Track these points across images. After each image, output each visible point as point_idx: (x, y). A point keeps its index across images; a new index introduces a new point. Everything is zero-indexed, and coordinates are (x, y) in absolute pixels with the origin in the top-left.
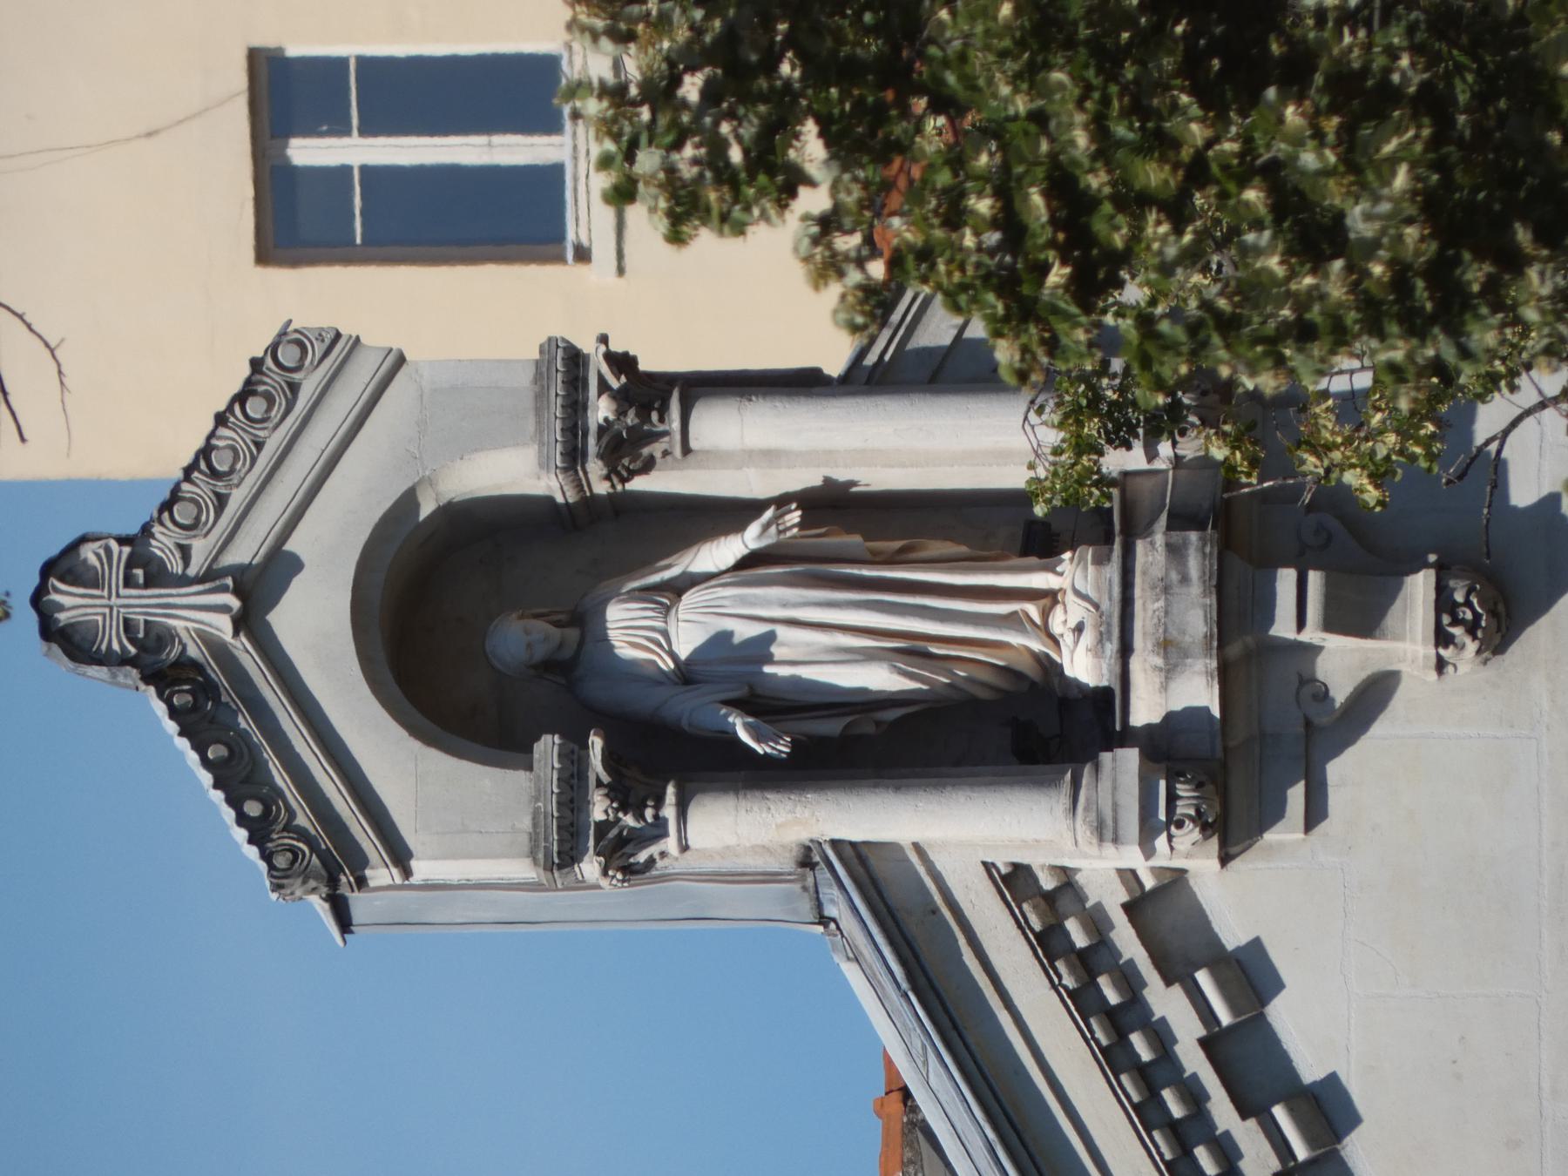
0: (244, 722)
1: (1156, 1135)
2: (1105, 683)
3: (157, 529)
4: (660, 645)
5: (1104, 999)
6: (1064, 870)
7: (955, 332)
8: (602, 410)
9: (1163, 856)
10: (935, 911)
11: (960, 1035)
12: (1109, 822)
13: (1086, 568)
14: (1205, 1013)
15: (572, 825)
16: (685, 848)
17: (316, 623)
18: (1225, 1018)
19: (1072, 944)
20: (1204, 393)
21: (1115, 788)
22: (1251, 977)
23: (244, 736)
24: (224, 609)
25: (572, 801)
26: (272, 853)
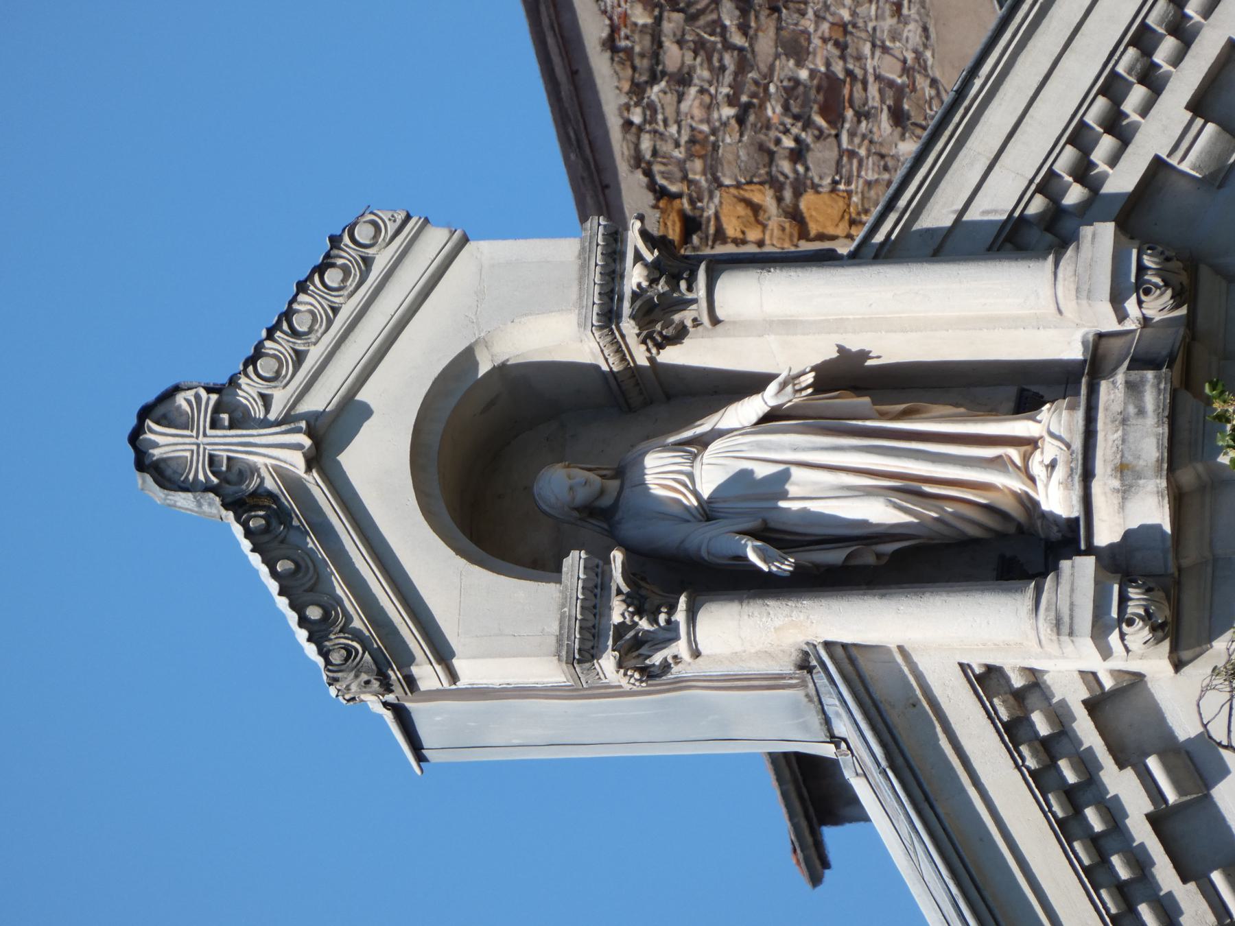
0: (312, 543)
1: (1104, 893)
2: (1075, 514)
3: (243, 381)
4: (686, 486)
5: (1063, 778)
6: (1032, 671)
7: (954, 216)
8: (635, 276)
9: (1120, 661)
10: (915, 704)
11: (932, 807)
12: (1066, 619)
13: (1060, 414)
14: (1154, 792)
15: (594, 627)
16: (696, 654)
17: (380, 463)
18: (1171, 796)
19: (1036, 733)
20: (1168, 259)
21: (1072, 590)
22: (1198, 764)
23: (310, 554)
24: (298, 447)
25: (595, 607)
26: (329, 651)
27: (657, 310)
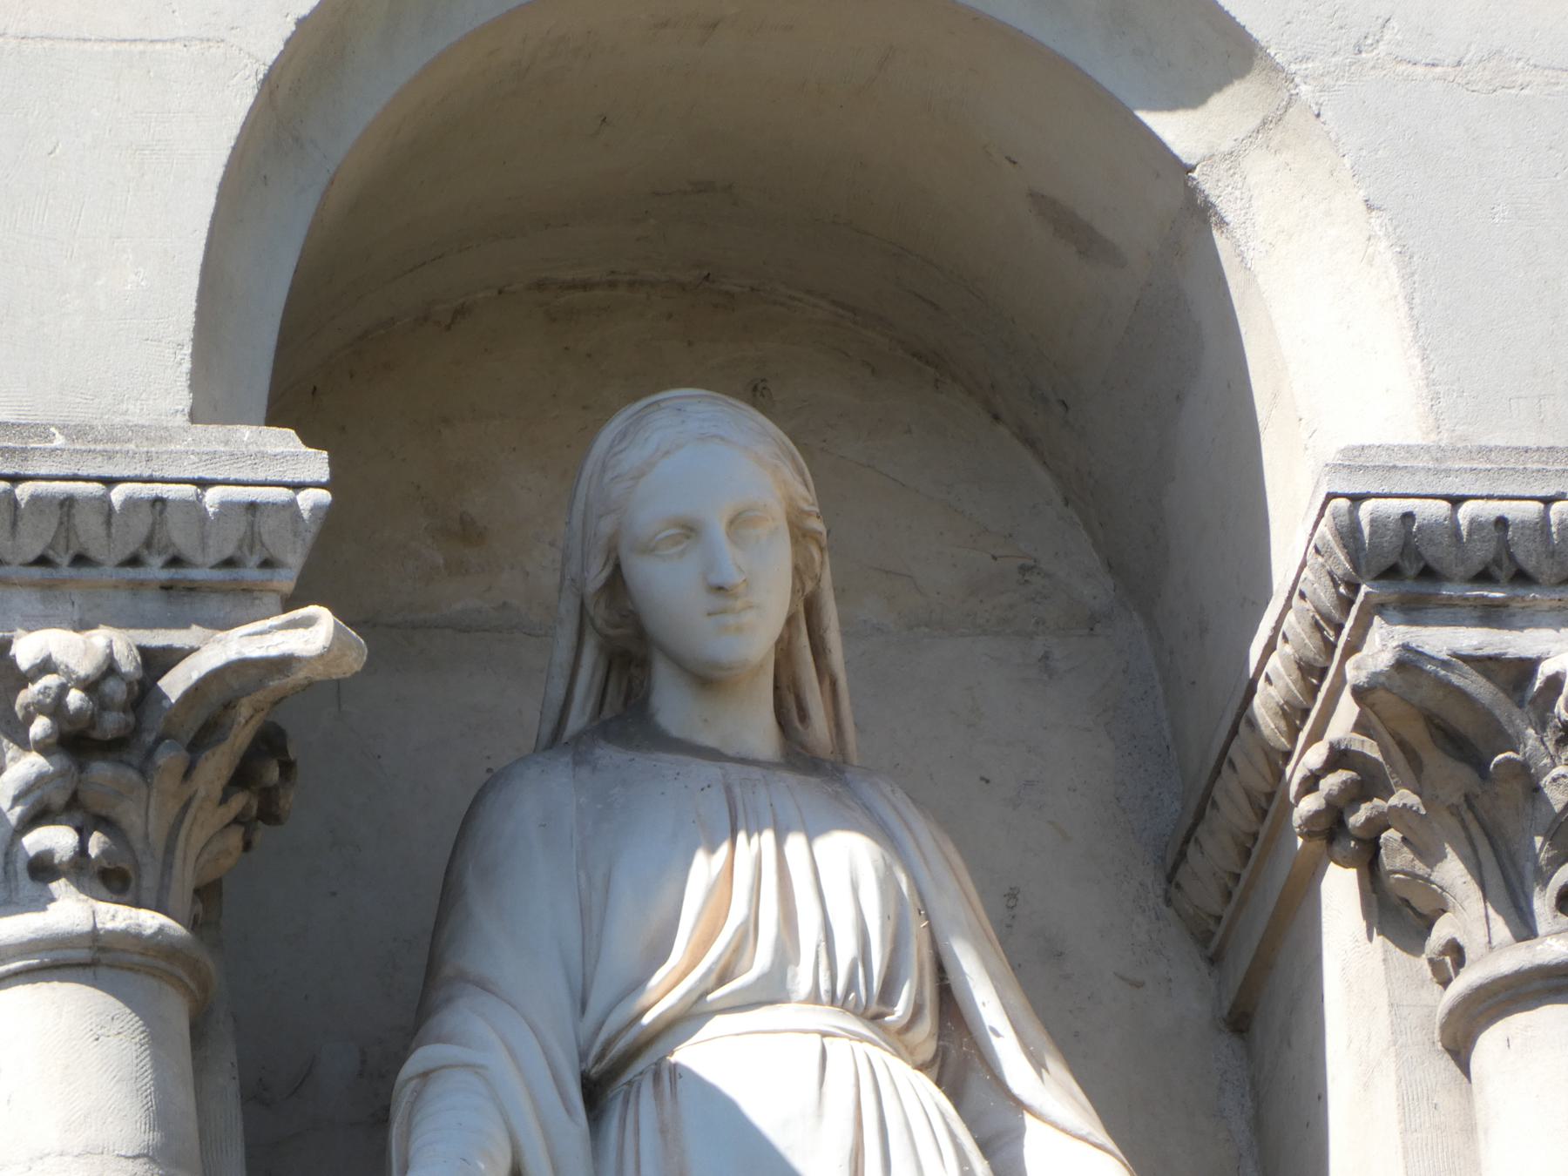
27: (1465, 775)
